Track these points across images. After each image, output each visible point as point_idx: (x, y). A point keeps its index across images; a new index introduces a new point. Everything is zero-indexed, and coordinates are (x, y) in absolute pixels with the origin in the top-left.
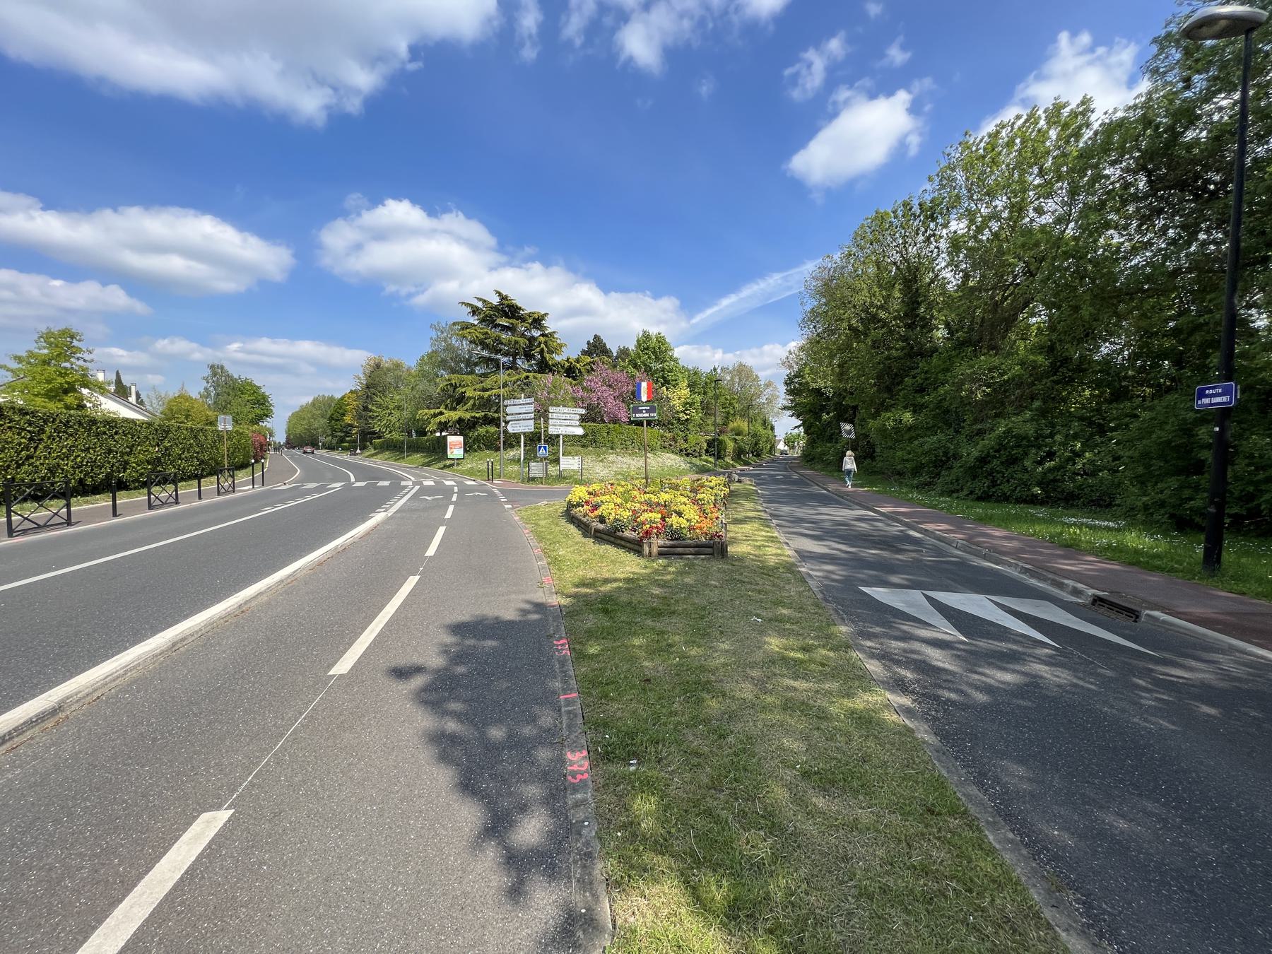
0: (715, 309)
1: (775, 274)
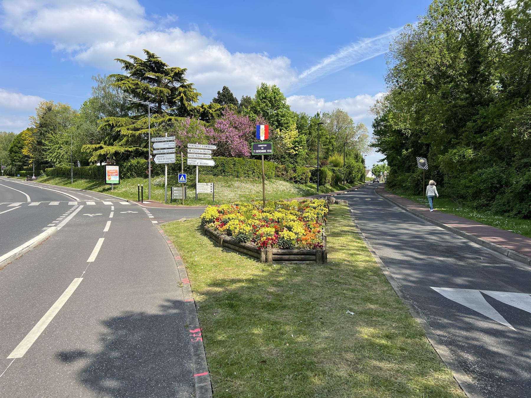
0: (319, 66)
1: (366, 39)
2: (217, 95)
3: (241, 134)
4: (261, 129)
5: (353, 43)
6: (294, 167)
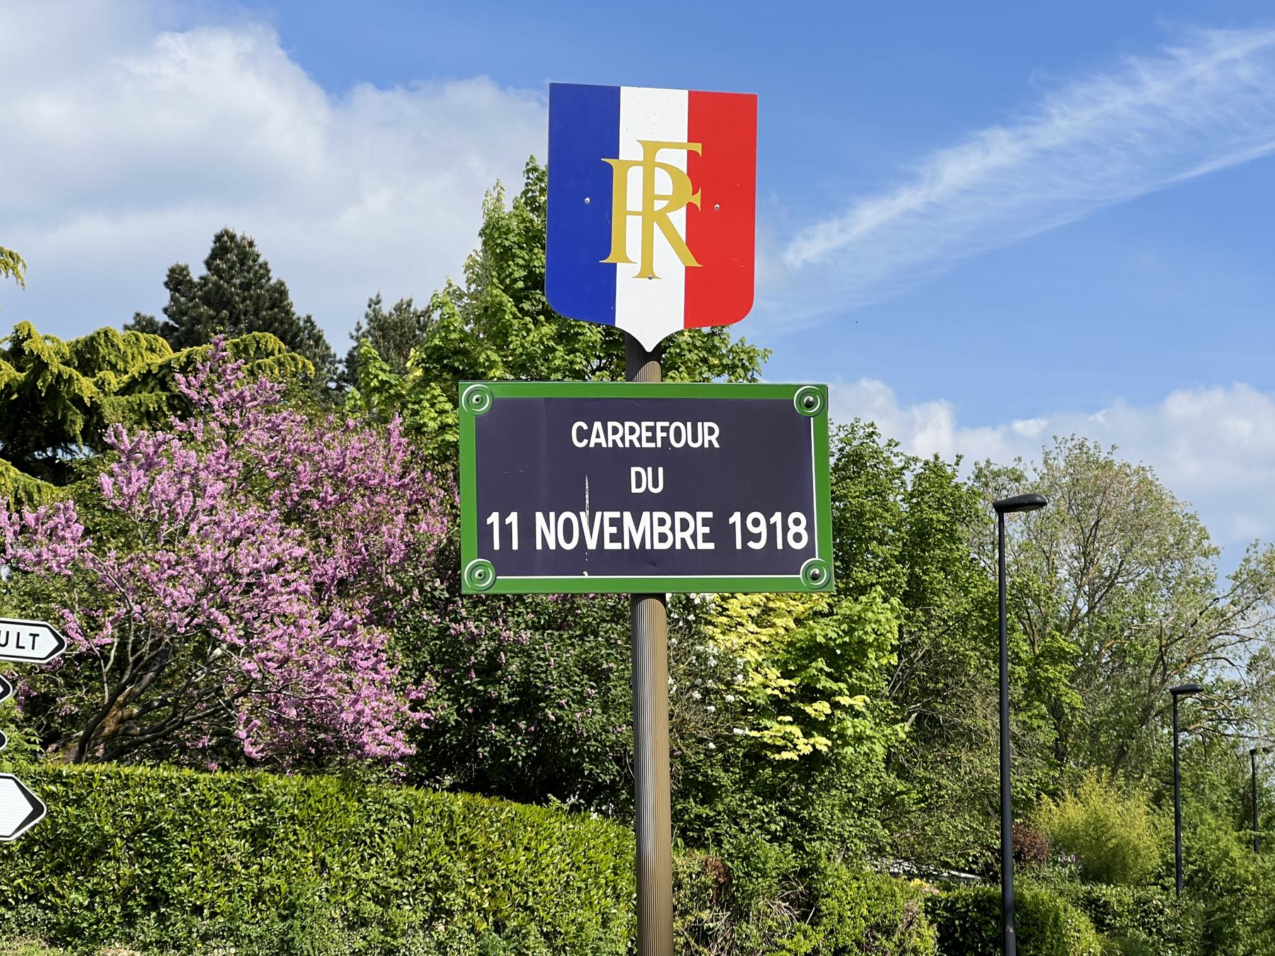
0: (907, 200)
1: (1217, 37)
2: (165, 297)
3: (337, 564)
4: (629, 147)
5: (1132, 60)
6: (803, 873)
